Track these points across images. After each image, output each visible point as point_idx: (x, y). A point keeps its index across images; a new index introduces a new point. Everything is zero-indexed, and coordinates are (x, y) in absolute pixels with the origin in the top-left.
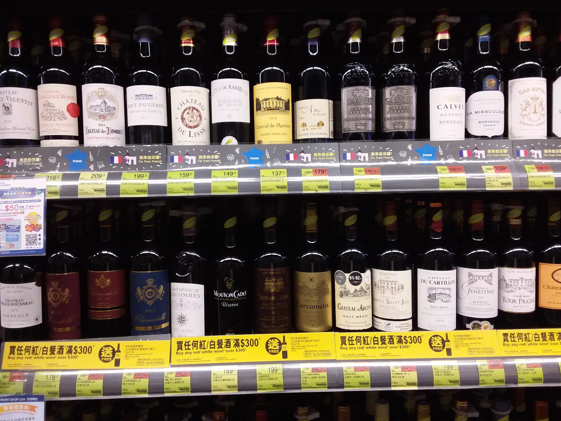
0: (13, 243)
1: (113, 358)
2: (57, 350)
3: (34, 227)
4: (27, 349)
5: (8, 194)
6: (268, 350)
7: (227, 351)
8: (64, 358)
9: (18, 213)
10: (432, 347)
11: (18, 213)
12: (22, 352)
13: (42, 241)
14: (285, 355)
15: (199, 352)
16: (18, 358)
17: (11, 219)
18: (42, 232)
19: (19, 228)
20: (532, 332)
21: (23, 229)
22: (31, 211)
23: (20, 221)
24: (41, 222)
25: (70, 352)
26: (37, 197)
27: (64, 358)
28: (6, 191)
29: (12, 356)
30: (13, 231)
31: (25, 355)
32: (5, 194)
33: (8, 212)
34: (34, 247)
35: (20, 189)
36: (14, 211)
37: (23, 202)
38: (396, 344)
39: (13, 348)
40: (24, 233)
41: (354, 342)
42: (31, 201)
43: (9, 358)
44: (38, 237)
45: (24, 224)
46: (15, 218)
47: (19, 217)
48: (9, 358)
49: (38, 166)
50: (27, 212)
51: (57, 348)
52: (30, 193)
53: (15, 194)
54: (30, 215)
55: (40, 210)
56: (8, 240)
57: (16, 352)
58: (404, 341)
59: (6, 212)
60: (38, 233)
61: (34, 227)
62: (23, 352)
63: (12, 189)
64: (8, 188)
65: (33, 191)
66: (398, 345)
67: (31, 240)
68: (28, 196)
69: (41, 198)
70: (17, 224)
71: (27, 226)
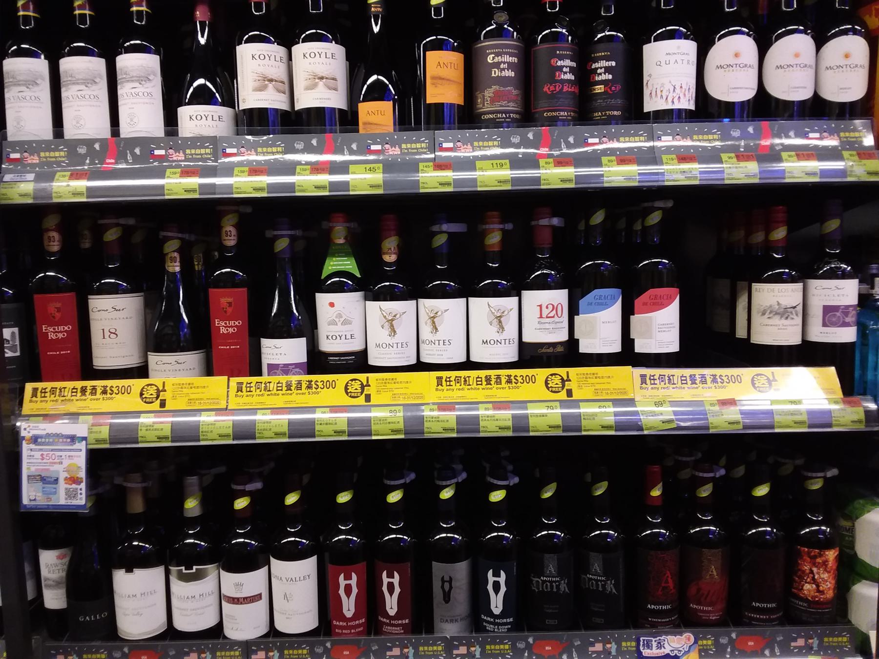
0: (51, 496)
1: (157, 398)
2: (89, 391)
3: (75, 480)
4: (53, 391)
5: (43, 440)
6: (347, 393)
7: (297, 394)
8: (97, 399)
9: (55, 463)
10: (548, 388)
11: (55, 463)
12: (47, 395)
13: (84, 496)
14: (368, 398)
15: (263, 395)
16: (41, 401)
17: (48, 470)
18: (83, 486)
19: (56, 481)
20: (677, 372)
21: (61, 481)
22: (71, 462)
23: (58, 472)
24: (82, 474)
25: (104, 392)
26: (77, 446)
27: (97, 399)
28: (41, 437)
29: (34, 399)
30: (49, 483)
31: (49, 397)
32: (39, 440)
33: (45, 461)
34: (75, 502)
35: (58, 436)
36: (51, 460)
37: (61, 450)
38: (504, 384)
39: (35, 390)
40: (62, 486)
41: (453, 383)
42: (70, 450)
43: (31, 401)
44: (79, 492)
45: (63, 476)
46: (52, 468)
47: (56, 467)
48: (31, 401)
49: (63, 162)
50: (66, 463)
51: (88, 388)
52: (69, 440)
53: (51, 440)
54: (70, 465)
55: (80, 461)
56: (44, 493)
57: (39, 394)
58: (514, 380)
59: (40, 461)
60: (79, 487)
61: (75, 480)
62: (48, 395)
63: (48, 435)
64: (44, 433)
65: (73, 439)
66: (506, 386)
67: (71, 494)
68: (66, 443)
69: (82, 446)
70: (54, 476)
71: (66, 479)
